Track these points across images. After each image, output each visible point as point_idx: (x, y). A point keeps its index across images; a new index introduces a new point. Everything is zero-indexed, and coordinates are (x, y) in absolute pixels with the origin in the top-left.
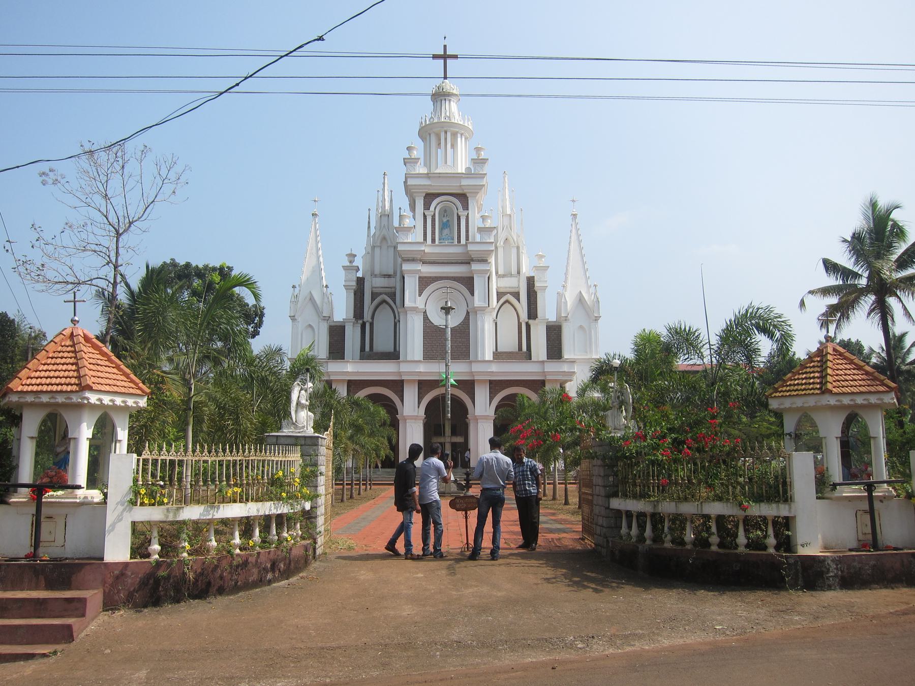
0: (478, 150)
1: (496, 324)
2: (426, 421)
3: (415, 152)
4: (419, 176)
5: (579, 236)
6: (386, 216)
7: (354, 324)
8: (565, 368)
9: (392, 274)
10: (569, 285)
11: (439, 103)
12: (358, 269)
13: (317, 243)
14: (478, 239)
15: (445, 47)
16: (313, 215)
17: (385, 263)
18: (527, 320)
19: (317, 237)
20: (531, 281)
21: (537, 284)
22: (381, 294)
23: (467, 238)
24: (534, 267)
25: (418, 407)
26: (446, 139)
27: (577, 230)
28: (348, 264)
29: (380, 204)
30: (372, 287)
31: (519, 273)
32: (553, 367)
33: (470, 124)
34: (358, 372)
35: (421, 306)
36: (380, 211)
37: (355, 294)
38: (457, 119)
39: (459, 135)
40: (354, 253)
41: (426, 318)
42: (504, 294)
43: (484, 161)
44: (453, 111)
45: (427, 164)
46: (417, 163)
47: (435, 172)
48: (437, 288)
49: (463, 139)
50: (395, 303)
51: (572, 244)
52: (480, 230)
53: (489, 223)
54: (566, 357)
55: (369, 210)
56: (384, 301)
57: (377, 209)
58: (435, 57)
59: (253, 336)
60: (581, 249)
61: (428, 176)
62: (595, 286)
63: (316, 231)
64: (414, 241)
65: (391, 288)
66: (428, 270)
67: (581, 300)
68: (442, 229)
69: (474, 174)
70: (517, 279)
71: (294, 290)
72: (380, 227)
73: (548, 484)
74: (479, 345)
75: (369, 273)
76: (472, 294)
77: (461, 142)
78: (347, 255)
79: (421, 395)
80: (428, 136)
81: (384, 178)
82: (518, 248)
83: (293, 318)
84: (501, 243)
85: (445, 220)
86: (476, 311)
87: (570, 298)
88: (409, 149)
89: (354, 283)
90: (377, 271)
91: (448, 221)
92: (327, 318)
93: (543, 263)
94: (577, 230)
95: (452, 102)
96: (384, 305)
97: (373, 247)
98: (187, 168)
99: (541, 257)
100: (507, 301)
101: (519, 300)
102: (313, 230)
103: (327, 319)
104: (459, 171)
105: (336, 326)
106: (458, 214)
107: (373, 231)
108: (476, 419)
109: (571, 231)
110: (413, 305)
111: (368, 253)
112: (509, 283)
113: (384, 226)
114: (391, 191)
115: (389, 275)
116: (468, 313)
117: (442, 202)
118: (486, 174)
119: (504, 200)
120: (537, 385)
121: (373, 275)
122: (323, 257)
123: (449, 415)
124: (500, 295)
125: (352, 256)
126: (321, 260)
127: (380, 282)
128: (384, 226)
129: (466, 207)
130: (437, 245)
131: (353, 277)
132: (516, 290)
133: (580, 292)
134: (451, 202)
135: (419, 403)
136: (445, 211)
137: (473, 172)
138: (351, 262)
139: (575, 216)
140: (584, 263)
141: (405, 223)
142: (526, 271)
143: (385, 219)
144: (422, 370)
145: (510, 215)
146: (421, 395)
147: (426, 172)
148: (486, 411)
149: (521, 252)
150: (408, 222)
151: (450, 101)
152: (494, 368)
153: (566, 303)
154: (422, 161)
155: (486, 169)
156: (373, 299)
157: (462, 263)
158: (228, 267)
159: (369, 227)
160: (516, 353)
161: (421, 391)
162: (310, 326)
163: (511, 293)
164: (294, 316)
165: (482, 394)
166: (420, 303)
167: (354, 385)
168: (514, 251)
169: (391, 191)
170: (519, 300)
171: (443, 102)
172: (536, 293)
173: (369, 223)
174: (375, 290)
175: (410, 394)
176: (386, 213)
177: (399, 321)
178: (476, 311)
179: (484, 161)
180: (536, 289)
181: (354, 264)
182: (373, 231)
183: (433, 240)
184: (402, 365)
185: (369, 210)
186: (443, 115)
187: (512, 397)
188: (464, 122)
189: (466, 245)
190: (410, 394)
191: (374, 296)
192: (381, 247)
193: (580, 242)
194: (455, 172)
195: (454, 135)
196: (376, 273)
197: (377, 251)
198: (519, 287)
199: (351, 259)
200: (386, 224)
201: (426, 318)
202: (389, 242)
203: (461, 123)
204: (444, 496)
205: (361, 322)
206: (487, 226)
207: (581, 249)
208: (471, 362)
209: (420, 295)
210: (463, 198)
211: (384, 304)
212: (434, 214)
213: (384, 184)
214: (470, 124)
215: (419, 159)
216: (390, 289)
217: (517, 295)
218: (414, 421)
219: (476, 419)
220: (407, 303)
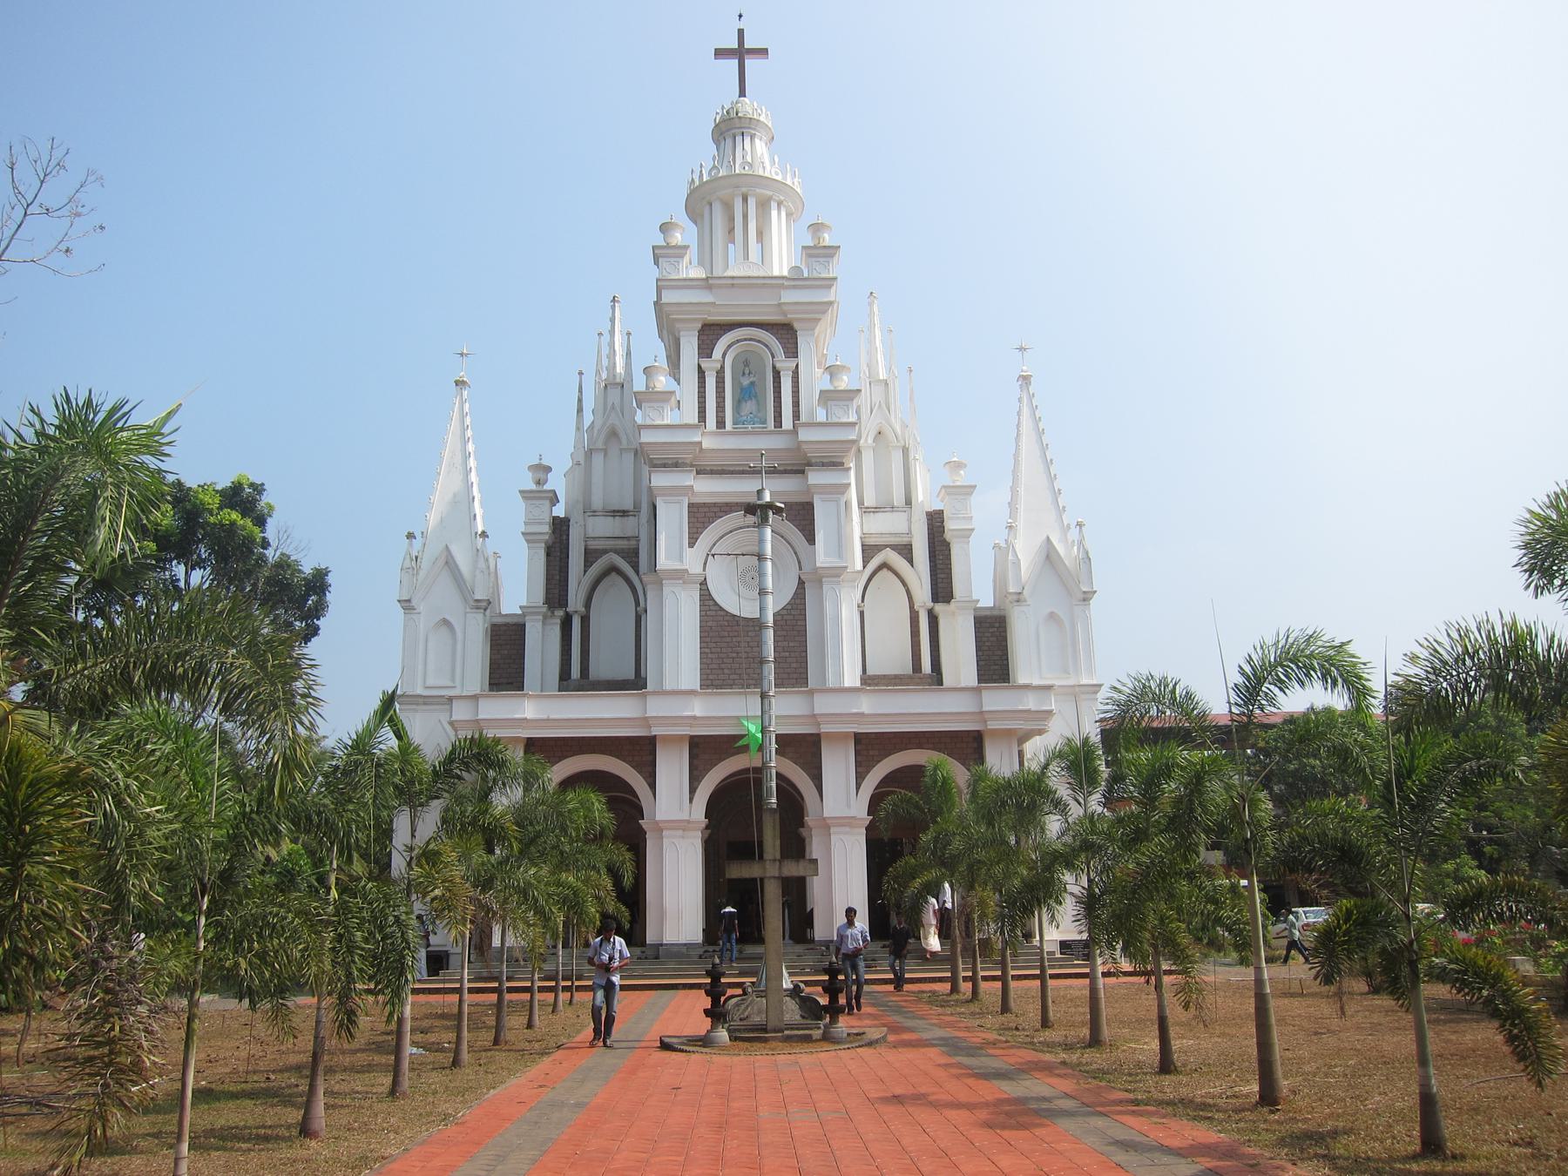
0: (816, 228)
1: (862, 614)
2: (710, 836)
3: (678, 235)
4: (688, 284)
5: (1037, 421)
6: (614, 387)
7: (545, 617)
8: (1031, 703)
9: (631, 508)
10: (1021, 524)
11: (729, 141)
12: (554, 500)
13: (465, 442)
14: (821, 416)
15: (741, 32)
16: (457, 383)
17: (614, 485)
18: (930, 604)
19: (464, 429)
20: (935, 521)
21: (950, 525)
22: (605, 552)
23: (796, 415)
24: (944, 487)
25: (691, 800)
26: (745, 216)
27: (1034, 409)
28: (533, 487)
29: (605, 362)
30: (587, 539)
31: (909, 502)
32: (996, 700)
33: (796, 183)
34: (548, 720)
35: (695, 568)
36: (604, 376)
37: (548, 555)
38: (770, 171)
39: (774, 205)
40: (545, 462)
41: (706, 597)
42: (879, 548)
43: (830, 252)
44: (759, 156)
45: (706, 258)
46: (682, 256)
47: (725, 274)
48: (730, 528)
49: (783, 214)
50: (637, 572)
51: (1024, 439)
52: (827, 397)
53: (844, 383)
54: (1022, 680)
55: (581, 373)
56: (613, 569)
57: (598, 372)
58: (720, 53)
59: (307, 639)
60: (1044, 448)
61: (707, 284)
62: (1080, 525)
63: (463, 416)
64: (677, 422)
65: (628, 538)
66: (709, 488)
67: (1049, 556)
68: (739, 401)
69: (806, 279)
70: (903, 516)
71: (411, 545)
72: (605, 408)
73: (985, 978)
74: (830, 662)
75: (580, 507)
76: (811, 539)
77: (777, 219)
78: (530, 468)
79: (695, 773)
80: (708, 207)
81: (613, 308)
82: (905, 451)
83: (407, 605)
84: (867, 440)
85: (746, 382)
86: (819, 577)
87: (1026, 552)
88: (665, 228)
89: (546, 529)
90: (597, 502)
91: (752, 383)
92: (485, 604)
93: (962, 478)
94: (1034, 409)
95: (757, 141)
96: (614, 576)
97: (589, 453)
98: (91, 178)
99: (959, 466)
100: (884, 566)
101: (911, 561)
102: (456, 415)
103: (484, 605)
104: (776, 273)
105: (506, 625)
106: (774, 367)
107: (588, 418)
108: (826, 825)
109: (1019, 414)
110: (677, 566)
111: (578, 464)
112: (887, 525)
113: (613, 407)
114: (629, 334)
115: (624, 511)
116: (801, 583)
117: (738, 341)
118: (835, 279)
119: (871, 352)
120: (968, 745)
121: (589, 511)
122: (476, 459)
123: (774, 800)
124: (869, 551)
125: (542, 470)
126: (473, 477)
127: (603, 527)
128: (613, 407)
129: (792, 352)
130: (730, 433)
131: (544, 514)
132: (905, 540)
133: (1048, 538)
134: (759, 341)
135: (692, 791)
136: (746, 364)
137: (806, 275)
138: (538, 483)
139: (1025, 380)
140: (1052, 479)
141: (657, 385)
142: (926, 498)
143: (614, 395)
144: (698, 714)
145: (887, 384)
146: (695, 773)
147: (704, 276)
148: (849, 806)
149: (911, 457)
150: (663, 382)
151: (752, 137)
152: (867, 705)
153: (1017, 563)
154: (693, 253)
155: (835, 269)
156: (588, 563)
157: (785, 472)
158: (252, 485)
159: (580, 410)
160: (910, 677)
161: (696, 762)
162: (446, 622)
163: (894, 547)
164: (409, 601)
165: (838, 767)
166: (692, 560)
167: (545, 749)
168: (897, 457)
169: (629, 334)
170: (911, 561)
171: (739, 139)
172: (947, 545)
173: (580, 400)
174: (593, 545)
175: (672, 770)
176: (618, 380)
177: (646, 611)
178: (819, 577)
179: (830, 252)
180: (948, 536)
181: (546, 487)
182: (588, 418)
183: (721, 423)
184: (651, 701)
185: (581, 373)
186: (739, 161)
187: (916, 771)
188: (785, 178)
189: (795, 431)
190: (672, 770)
191: (590, 556)
192: (605, 451)
193: (1040, 433)
194: (766, 275)
195: (764, 205)
196: (594, 507)
197: (598, 460)
198: (910, 533)
199: (541, 475)
200: (617, 401)
201: (706, 597)
202: (624, 442)
203: (779, 178)
204: (765, 1040)
205: (560, 613)
206: (842, 388)
207: (1044, 448)
208: (811, 693)
209: (691, 545)
210: (786, 333)
211: (614, 574)
212: (723, 367)
213: (613, 320)
214: (796, 183)
215: (686, 247)
216: (626, 542)
217: (906, 551)
218: (680, 832)
219: (826, 825)
220: (663, 562)
